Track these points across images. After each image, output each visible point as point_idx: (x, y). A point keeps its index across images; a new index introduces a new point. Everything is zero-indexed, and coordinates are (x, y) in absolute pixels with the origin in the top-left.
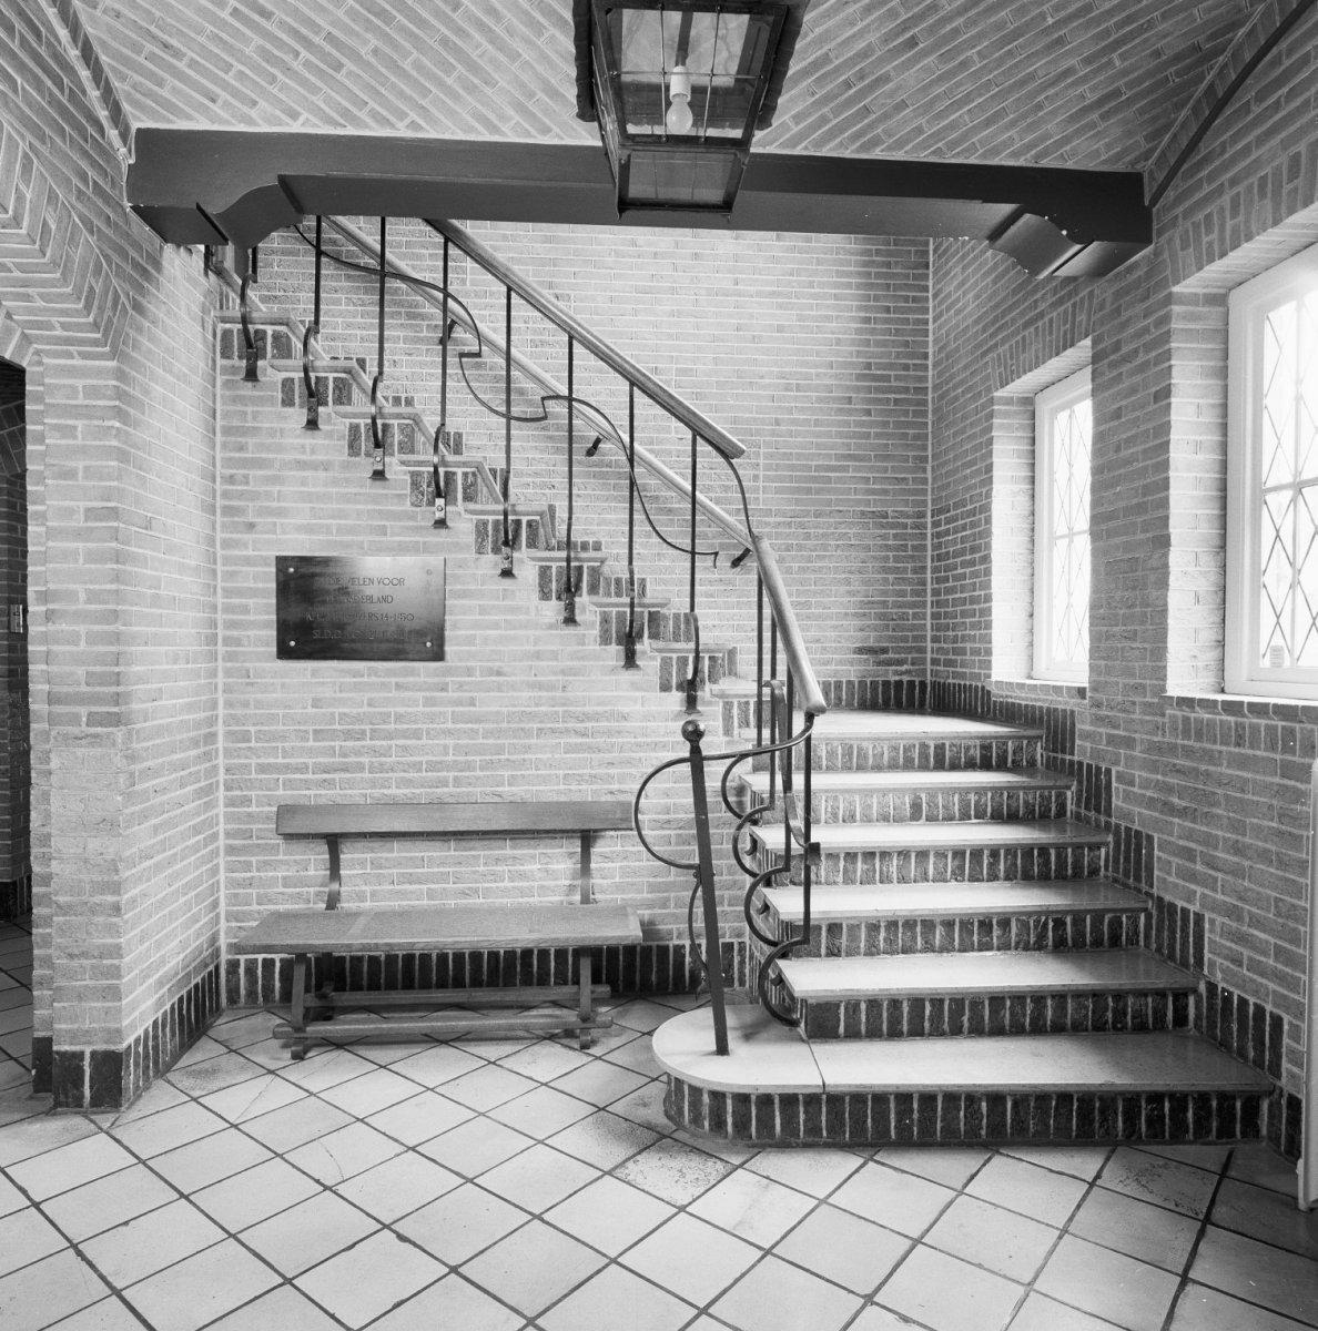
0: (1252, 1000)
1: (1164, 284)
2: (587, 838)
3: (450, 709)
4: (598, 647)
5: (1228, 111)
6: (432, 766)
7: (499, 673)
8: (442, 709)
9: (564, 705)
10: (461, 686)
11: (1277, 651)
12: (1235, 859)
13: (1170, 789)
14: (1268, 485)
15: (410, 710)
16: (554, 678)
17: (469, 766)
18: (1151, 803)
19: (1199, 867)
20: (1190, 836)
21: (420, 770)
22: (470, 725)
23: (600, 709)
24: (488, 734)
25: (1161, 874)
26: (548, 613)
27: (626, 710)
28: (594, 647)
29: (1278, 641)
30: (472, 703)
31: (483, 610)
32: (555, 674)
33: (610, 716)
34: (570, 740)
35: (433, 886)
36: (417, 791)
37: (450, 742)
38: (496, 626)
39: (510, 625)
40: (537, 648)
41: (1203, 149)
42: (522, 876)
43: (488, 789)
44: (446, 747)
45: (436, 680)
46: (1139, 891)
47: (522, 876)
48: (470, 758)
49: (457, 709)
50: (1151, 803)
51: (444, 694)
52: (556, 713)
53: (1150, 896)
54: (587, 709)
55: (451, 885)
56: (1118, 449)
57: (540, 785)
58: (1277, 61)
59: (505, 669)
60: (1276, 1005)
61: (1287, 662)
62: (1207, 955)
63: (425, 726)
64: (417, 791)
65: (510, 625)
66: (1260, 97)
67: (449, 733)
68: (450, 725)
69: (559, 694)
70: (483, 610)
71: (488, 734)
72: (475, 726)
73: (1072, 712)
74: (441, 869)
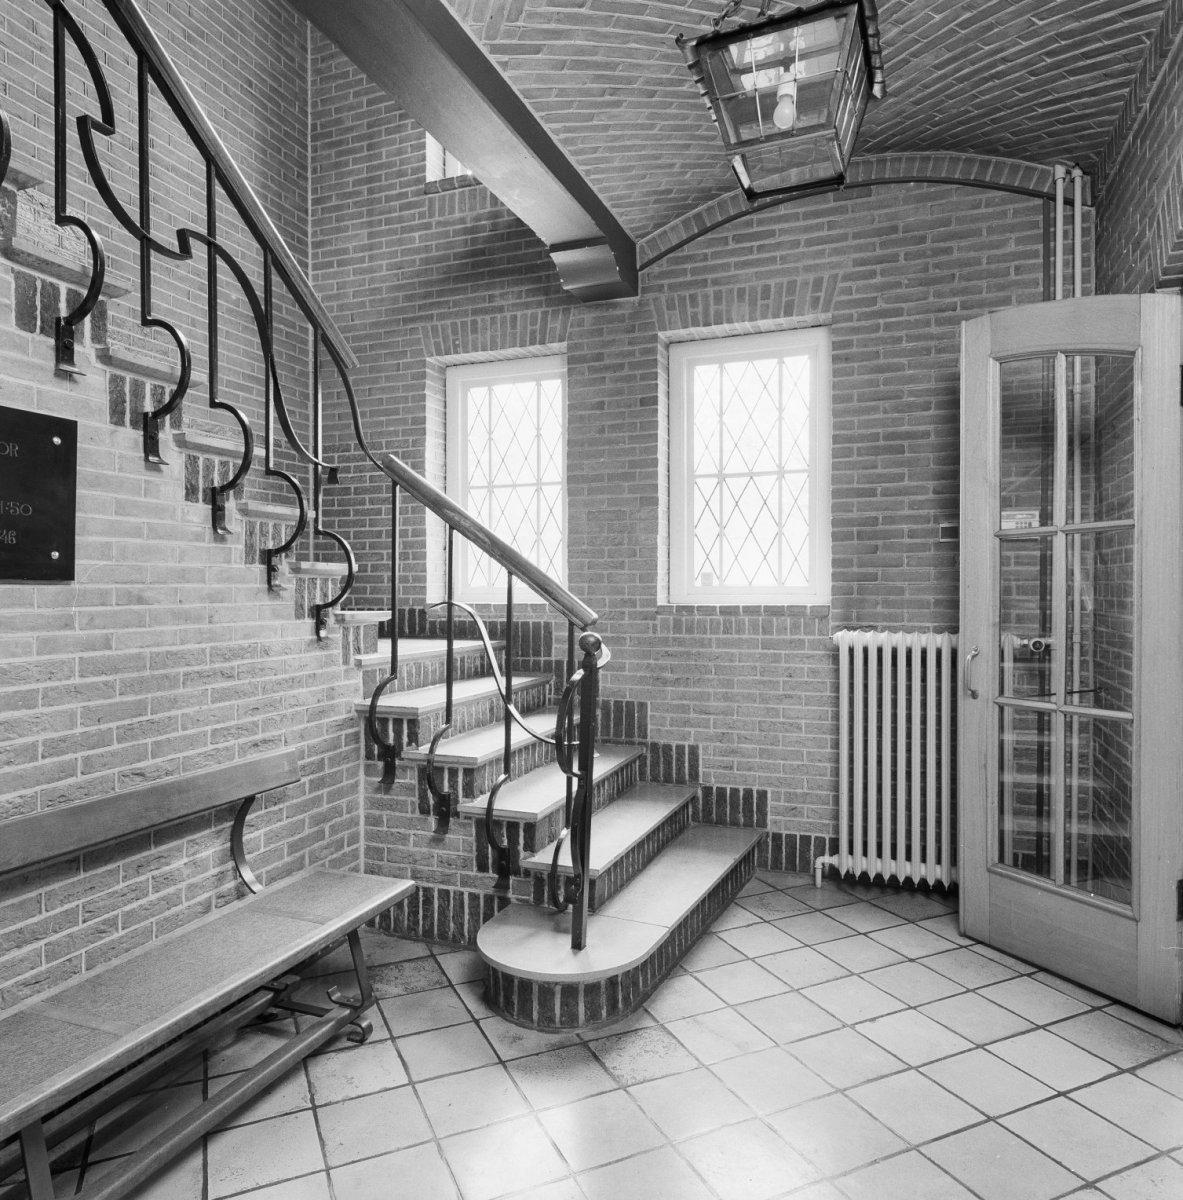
0: (741, 788)
1: (649, 326)
2: (239, 811)
3: (77, 656)
4: (243, 566)
5: (709, 236)
6: (53, 748)
7: (140, 600)
8: (64, 656)
9: (211, 640)
10: (91, 621)
11: (707, 577)
12: (727, 704)
13: (663, 669)
14: (697, 473)
15: (17, 661)
16: (198, 605)
17: (103, 740)
18: (642, 680)
19: (692, 715)
20: (683, 697)
21: (34, 758)
22: (104, 678)
23: (245, 643)
24: (128, 687)
25: (654, 727)
26: (195, 519)
27: (266, 641)
28: (238, 565)
29: (708, 569)
30: (107, 644)
31: (121, 508)
32: (202, 600)
33: (251, 651)
34: (216, 686)
35: (54, 937)
36: (28, 792)
37: (76, 706)
38: (136, 532)
39: (154, 532)
40: (183, 565)
41: (686, 250)
42: (169, 880)
43: (126, 768)
44: (72, 715)
45: (58, 611)
46: (633, 743)
47: (169, 880)
48: (103, 727)
49: (86, 655)
50: (642, 680)
51: (68, 633)
52: (203, 650)
53: (645, 744)
54: (233, 644)
55: (82, 926)
56: (602, 431)
57: (187, 749)
58: (749, 224)
59: (147, 594)
60: (761, 785)
61: (716, 582)
62: (701, 769)
63: (41, 686)
64: (28, 792)
65: (154, 532)
66: (738, 239)
67: (77, 691)
68: (77, 680)
69: (205, 626)
70: (121, 508)
71: (128, 687)
72: (110, 678)
73: (547, 625)
74: (67, 907)
